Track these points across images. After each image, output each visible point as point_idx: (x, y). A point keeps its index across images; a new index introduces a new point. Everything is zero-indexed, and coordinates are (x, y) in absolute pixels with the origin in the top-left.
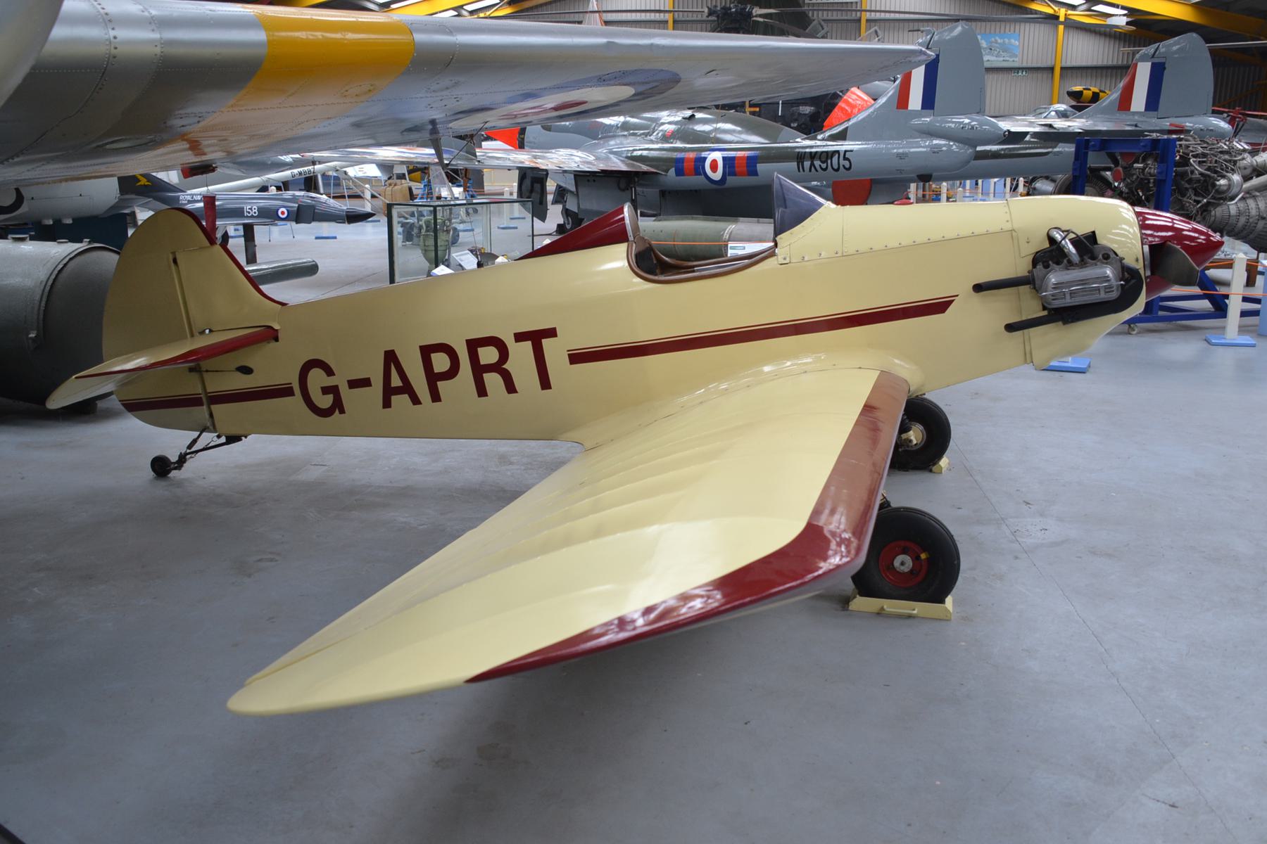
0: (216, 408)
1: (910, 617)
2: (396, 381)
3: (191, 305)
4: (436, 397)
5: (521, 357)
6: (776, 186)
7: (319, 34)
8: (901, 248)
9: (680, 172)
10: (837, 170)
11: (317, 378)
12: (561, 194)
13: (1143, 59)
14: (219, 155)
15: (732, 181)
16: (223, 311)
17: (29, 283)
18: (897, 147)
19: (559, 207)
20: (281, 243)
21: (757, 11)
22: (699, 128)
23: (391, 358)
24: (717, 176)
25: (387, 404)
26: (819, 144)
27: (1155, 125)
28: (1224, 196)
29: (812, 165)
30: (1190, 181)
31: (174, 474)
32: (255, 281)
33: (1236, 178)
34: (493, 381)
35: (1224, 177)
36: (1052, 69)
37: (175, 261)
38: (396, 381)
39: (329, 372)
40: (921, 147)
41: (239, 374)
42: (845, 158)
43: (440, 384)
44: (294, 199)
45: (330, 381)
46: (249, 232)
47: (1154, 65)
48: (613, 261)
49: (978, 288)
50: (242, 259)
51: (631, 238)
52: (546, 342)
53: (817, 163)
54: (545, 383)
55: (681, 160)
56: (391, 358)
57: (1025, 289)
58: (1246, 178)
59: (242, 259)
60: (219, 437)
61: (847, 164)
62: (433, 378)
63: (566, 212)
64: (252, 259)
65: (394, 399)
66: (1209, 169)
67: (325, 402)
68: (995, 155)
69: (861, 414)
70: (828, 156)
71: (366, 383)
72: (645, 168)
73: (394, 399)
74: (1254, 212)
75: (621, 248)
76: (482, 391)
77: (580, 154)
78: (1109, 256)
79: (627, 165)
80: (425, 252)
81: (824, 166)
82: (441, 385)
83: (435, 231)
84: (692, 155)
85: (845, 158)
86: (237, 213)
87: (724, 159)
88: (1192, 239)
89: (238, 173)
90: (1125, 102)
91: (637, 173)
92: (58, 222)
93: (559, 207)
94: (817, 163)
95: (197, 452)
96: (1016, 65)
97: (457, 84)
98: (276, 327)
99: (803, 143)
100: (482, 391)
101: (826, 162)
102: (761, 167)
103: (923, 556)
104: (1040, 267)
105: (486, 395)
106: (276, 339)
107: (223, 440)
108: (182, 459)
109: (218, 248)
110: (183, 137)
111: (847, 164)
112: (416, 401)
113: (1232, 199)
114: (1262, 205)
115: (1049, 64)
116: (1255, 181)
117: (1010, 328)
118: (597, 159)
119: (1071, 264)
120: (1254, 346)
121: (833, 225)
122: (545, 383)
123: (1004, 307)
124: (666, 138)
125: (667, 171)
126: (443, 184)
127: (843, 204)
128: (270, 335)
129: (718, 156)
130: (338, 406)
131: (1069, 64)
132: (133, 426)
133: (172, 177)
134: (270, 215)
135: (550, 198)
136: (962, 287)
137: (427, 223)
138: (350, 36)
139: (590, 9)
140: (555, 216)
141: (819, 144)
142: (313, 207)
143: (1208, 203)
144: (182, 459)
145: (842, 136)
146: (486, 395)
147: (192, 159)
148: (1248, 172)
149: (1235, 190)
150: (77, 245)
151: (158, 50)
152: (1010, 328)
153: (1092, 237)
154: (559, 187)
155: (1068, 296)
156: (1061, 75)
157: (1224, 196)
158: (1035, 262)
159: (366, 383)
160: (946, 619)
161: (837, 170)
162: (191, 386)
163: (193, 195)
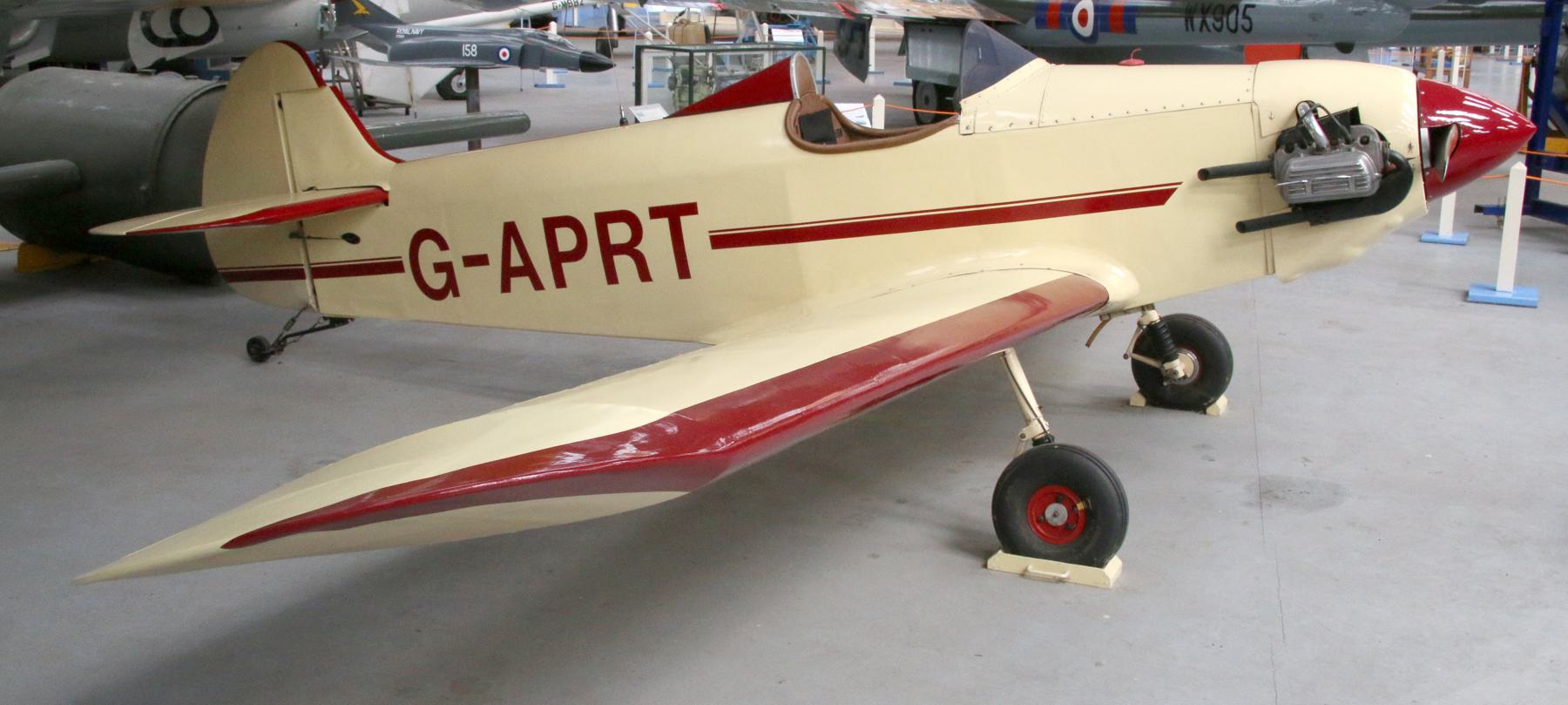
1: (1060, 581)
2: (516, 261)
3: (296, 160)
4: (560, 282)
5: (656, 235)
10: (1235, 31)
11: (429, 250)
23: (511, 231)
24: (1086, 32)
25: (506, 287)
29: (1204, 22)
34: (623, 263)
38: (516, 261)
39: (443, 246)
41: (345, 244)
42: (1245, 17)
45: (444, 257)
49: (1205, 175)
51: (797, 96)
52: (685, 221)
54: (684, 272)
56: (511, 231)
61: (1246, 23)
62: (558, 259)
65: (515, 281)
67: (437, 281)
68: (1427, 17)
71: (481, 260)
73: (515, 281)
76: (612, 277)
81: (1218, 25)
82: (567, 267)
85: (1245, 17)
88: (1506, 124)
89: (467, 8)
94: (1210, 20)
95: (302, 333)
98: (386, 188)
100: (612, 277)
101: (1221, 20)
103: (1080, 506)
106: (386, 203)
109: (327, 90)
111: (1246, 23)
112: (538, 286)
117: (1243, 227)
119: (1319, 150)
122: (684, 272)
123: (1233, 201)
125: (1025, 21)
127: (1058, 62)
128: (379, 197)
130: (452, 287)
134: (490, 55)
136: (1189, 174)
142: (540, 48)
150: (206, 82)
152: (1243, 227)
153: (1352, 116)
155: (1309, 190)
159: (481, 260)
161: (1235, 31)
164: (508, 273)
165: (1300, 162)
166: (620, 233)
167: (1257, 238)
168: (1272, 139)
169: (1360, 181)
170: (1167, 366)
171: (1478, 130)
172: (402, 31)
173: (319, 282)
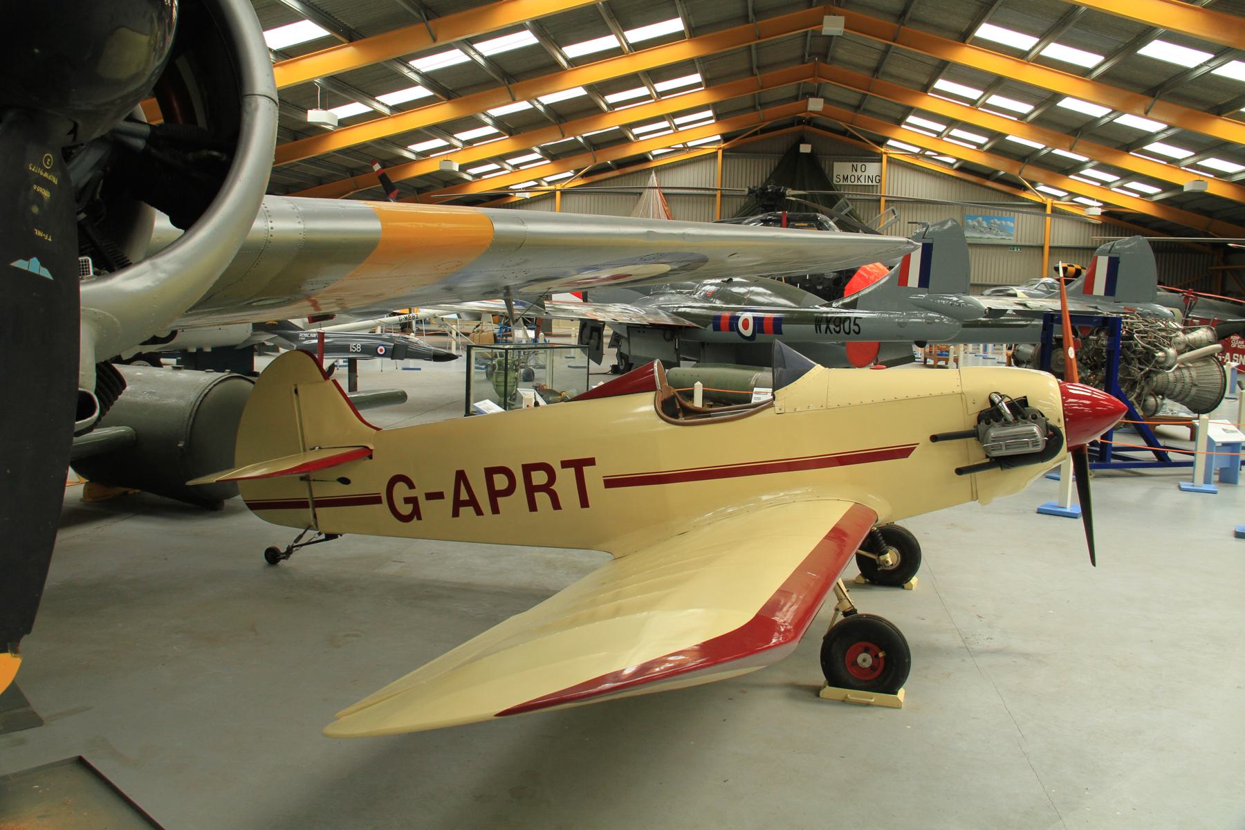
0: (319, 511)
1: (868, 705)
2: (464, 496)
4: (495, 510)
6: (776, 348)
7: (421, 224)
8: (873, 404)
9: (717, 328)
11: (401, 490)
12: (616, 340)
13: (1102, 253)
14: (336, 309)
15: (760, 338)
16: (327, 427)
17: (182, 403)
18: (896, 316)
19: (615, 350)
20: (378, 374)
21: (789, 192)
22: (736, 290)
23: (461, 476)
24: (748, 333)
25: (456, 513)
26: (835, 310)
27: (1106, 311)
28: (1162, 366)
29: (828, 328)
30: (1134, 352)
31: (282, 562)
32: (355, 405)
33: (1171, 351)
34: (542, 498)
35: (1161, 350)
36: (1042, 247)
37: (296, 391)
38: (464, 496)
39: (411, 486)
40: (918, 318)
41: (339, 484)
42: (855, 324)
43: (499, 499)
44: (391, 339)
46: (352, 365)
47: (1110, 259)
48: (644, 405)
49: (934, 438)
50: (346, 390)
51: (659, 388)
52: (586, 469)
53: (832, 327)
54: (584, 503)
55: (717, 318)
56: (461, 476)
57: (972, 440)
58: (1180, 352)
59: (344, 384)
60: (320, 534)
61: (856, 328)
62: (494, 495)
63: (621, 356)
64: (353, 387)
65: (462, 510)
66: (1149, 343)
67: (406, 509)
69: (827, 537)
70: (841, 321)
71: (440, 496)
72: (687, 323)
73: (462, 510)
74: (1188, 380)
75: (650, 396)
76: (533, 507)
77: (633, 309)
78: (1036, 417)
79: (673, 320)
80: (497, 386)
82: (500, 500)
83: (506, 369)
84: (727, 314)
85: (855, 324)
86: (344, 349)
87: (754, 318)
88: (1104, 406)
90: (1088, 287)
91: (680, 327)
92: (200, 350)
93: (615, 350)
94: (832, 327)
96: (1013, 243)
97: (526, 261)
98: (371, 447)
99: (820, 308)
100: (533, 507)
102: (784, 327)
103: (881, 655)
104: (983, 423)
105: (587, 506)
107: (323, 537)
108: (290, 551)
110: (308, 298)
111: (856, 328)
112: (479, 512)
113: (1170, 368)
114: (1194, 373)
115: (1039, 243)
116: (1187, 355)
117: (959, 471)
118: (647, 313)
119: (1007, 423)
120: (1215, 493)
121: (820, 382)
122: (584, 503)
123: (955, 454)
124: (707, 297)
126: (519, 327)
127: (830, 367)
128: (367, 453)
129: (749, 315)
130: (416, 513)
131: (1056, 244)
132: (252, 520)
133: (297, 322)
135: (606, 341)
137: (500, 363)
138: (444, 225)
139: (650, 185)
140: (610, 358)
141: (835, 310)
142: (406, 346)
143: (1150, 371)
144: (290, 551)
145: (852, 305)
146: (587, 506)
147: (313, 312)
148: (1182, 347)
149: (1170, 362)
150: (220, 374)
151: (301, 237)
152: (959, 471)
153: (1024, 402)
154: (615, 333)
156: (1050, 254)
157: (1162, 366)
158: (979, 419)
159: (440, 496)
160: (898, 706)
162: (301, 492)
163: (309, 334)
164: (458, 504)
165: (994, 432)
166: (539, 478)
167: (966, 476)
168: (975, 417)
169: (1035, 444)
170: (882, 558)
171: (1087, 410)
172: (302, 335)
173: (318, 510)
